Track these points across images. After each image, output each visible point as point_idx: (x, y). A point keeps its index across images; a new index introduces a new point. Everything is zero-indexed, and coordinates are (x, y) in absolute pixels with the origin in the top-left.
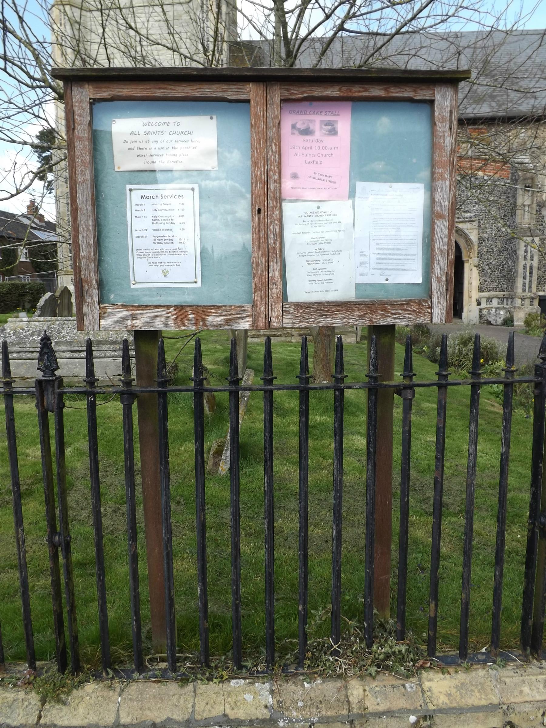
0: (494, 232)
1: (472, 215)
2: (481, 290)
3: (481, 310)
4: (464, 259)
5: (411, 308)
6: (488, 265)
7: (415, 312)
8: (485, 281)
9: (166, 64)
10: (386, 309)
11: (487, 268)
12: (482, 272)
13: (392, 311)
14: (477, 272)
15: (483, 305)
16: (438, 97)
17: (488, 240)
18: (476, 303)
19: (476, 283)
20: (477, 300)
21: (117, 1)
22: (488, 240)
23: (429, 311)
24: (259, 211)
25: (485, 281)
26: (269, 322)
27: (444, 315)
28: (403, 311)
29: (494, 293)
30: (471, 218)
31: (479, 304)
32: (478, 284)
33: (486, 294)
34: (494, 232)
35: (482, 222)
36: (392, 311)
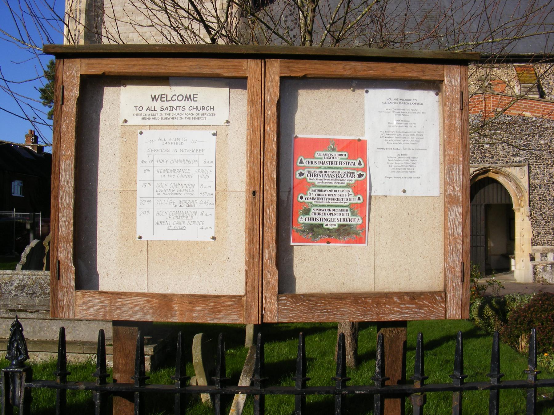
0: (546, 178)
1: (522, 159)
2: (534, 243)
3: (535, 267)
4: (514, 207)
5: (422, 302)
6: (541, 215)
7: (427, 306)
8: (539, 233)
9: (152, 42)
10: (395, 303)
11: (541, 218)
12: (534, 221)
13: (402, 306)
14: (530, 222)
15: (538, 259)
16: (447, 79)
17: (540, 188)
18: (529, 259)
19: (528, 236)
20: (531, 255)
21: (1, 352)
22: (540, 188)
23: (443, 305)
24: (254, 193)
25: (539, 233)
26: (262, 316)
27: (460, 310)
28: (414, 306)
29: (549, 247)
30: (520, 162)
31: (533, 259)
32: (531, 236)
33: (539, 247)
34: (546, 178)
35: (532, 167)
36: (402, 306)
